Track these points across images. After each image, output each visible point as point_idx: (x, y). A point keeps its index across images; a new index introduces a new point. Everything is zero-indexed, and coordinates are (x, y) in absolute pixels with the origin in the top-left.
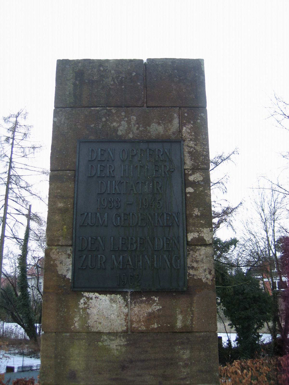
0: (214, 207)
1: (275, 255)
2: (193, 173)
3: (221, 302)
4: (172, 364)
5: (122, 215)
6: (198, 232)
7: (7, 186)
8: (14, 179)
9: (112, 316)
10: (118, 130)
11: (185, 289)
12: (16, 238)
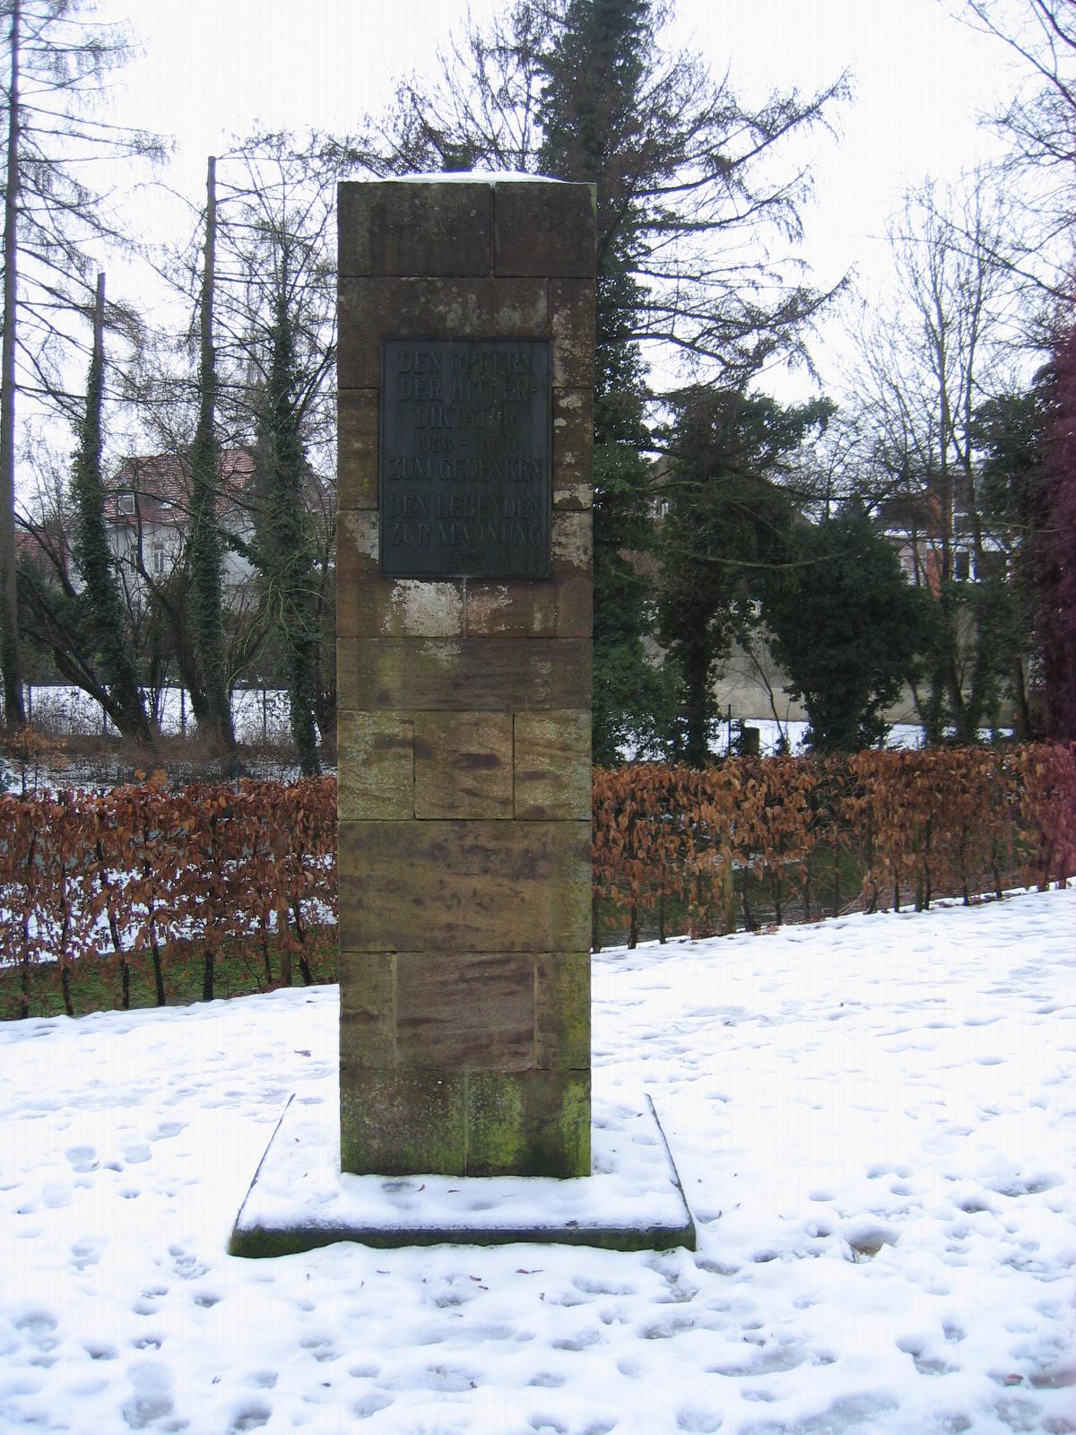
0: (757, 288)
1: (965, 460)
2: (567, 395)
3: (764, 615)
4: (525, 681)
5: (454, 462)
6: (570, 490)
7: (7, 202)
8: (31, 173)
9: (440, 613)
10: (446, 320)
11: (547, 575)
12: (55, 394)
